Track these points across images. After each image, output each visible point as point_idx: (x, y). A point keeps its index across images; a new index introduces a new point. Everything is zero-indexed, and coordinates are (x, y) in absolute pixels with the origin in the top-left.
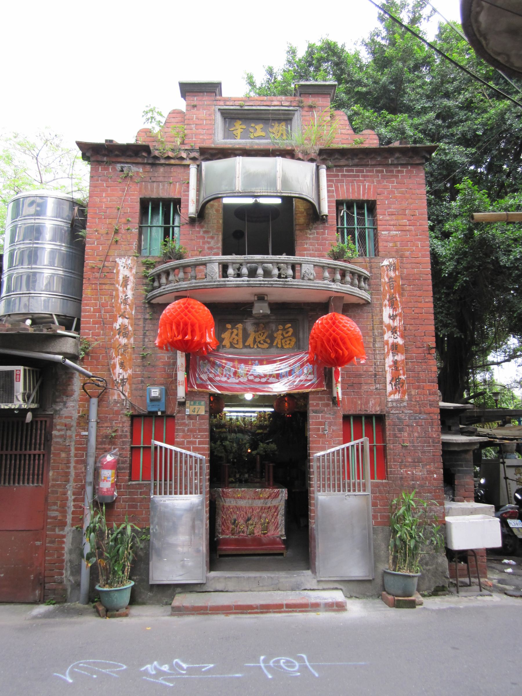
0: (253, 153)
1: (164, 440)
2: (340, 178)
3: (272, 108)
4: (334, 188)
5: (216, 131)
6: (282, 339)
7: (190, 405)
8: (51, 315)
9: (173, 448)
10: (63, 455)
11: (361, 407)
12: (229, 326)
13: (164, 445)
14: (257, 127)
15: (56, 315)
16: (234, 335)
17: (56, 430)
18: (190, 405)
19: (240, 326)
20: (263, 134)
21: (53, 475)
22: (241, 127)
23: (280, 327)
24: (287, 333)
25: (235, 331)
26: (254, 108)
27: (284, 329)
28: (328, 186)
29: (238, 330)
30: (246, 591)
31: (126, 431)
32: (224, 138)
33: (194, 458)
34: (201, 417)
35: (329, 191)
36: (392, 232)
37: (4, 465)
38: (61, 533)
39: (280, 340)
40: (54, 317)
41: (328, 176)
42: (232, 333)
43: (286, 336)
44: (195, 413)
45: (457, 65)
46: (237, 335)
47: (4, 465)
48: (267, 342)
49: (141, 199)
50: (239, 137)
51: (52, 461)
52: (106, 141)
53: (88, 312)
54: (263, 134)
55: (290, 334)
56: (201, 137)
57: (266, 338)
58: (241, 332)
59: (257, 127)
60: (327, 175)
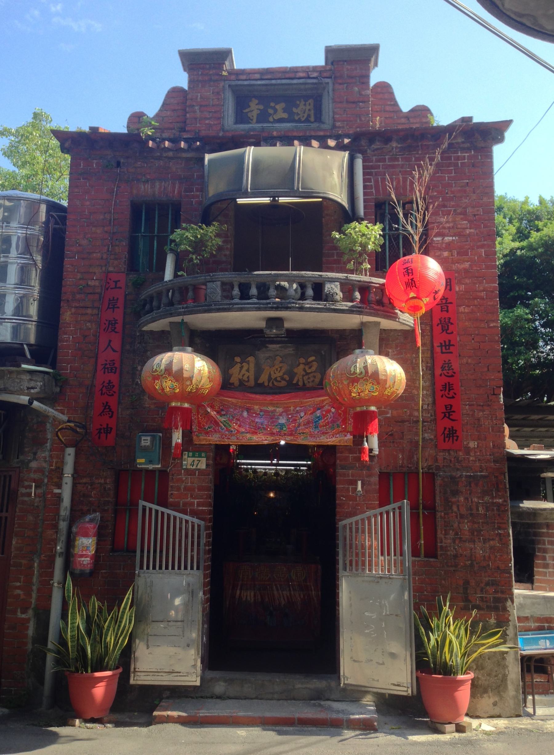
0: (308, 310)
1: (156, 501)
2: (381, 169)
3: (295, 81)
4: (372, 183)
5: (226, 113)
6: (303, 376)
7: (188, 457)
8: (22, 344)
9: (166, 511)
10: (31, 518)
11: (403, 462)
12: (238, 359)
13: (154, 507)
14: (277, 107)
15: (27, 345)
16: (244, 371)
17: (23, 487)
18: (188, 457)
19: (251, 359)
20: (285, 115)
21: (17, 543)
22: (257, 107)
23: (302, 360)
24: (310, 368)
25: (245, 368)
26: (273, 82)
27: (307, 363)
28: (365, 181)
29: (249, 364)
30: (252, 699)
31: (109, 489)
32: (236, 122)
33: (190, 524)
34: (201, 471)
35: (365, 187)
36: (446, 238)
37: (3, 525)
38: (23, 616)
39: (301, 377)
40: (25, 346)
41: (364, 168)
42: (242, 368)
43: (309, 371)
44: (194, 467)
45: (266, 748)
46: (248, 370)
47: (3, 525)
48: (285, 380)
49: (132, 202)
50: (255, 120)
51: (16, 526)
52: (91, 128)
53: (67, 341)
54: (285, 115)
55: (314, 369)
56: (207, 122)
57: (284, 374)
58: (252, 366)
59: (277, 107)
60: (363, 166)
